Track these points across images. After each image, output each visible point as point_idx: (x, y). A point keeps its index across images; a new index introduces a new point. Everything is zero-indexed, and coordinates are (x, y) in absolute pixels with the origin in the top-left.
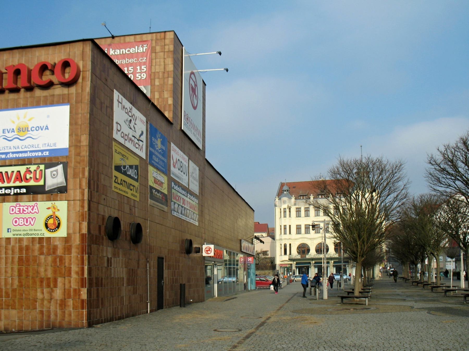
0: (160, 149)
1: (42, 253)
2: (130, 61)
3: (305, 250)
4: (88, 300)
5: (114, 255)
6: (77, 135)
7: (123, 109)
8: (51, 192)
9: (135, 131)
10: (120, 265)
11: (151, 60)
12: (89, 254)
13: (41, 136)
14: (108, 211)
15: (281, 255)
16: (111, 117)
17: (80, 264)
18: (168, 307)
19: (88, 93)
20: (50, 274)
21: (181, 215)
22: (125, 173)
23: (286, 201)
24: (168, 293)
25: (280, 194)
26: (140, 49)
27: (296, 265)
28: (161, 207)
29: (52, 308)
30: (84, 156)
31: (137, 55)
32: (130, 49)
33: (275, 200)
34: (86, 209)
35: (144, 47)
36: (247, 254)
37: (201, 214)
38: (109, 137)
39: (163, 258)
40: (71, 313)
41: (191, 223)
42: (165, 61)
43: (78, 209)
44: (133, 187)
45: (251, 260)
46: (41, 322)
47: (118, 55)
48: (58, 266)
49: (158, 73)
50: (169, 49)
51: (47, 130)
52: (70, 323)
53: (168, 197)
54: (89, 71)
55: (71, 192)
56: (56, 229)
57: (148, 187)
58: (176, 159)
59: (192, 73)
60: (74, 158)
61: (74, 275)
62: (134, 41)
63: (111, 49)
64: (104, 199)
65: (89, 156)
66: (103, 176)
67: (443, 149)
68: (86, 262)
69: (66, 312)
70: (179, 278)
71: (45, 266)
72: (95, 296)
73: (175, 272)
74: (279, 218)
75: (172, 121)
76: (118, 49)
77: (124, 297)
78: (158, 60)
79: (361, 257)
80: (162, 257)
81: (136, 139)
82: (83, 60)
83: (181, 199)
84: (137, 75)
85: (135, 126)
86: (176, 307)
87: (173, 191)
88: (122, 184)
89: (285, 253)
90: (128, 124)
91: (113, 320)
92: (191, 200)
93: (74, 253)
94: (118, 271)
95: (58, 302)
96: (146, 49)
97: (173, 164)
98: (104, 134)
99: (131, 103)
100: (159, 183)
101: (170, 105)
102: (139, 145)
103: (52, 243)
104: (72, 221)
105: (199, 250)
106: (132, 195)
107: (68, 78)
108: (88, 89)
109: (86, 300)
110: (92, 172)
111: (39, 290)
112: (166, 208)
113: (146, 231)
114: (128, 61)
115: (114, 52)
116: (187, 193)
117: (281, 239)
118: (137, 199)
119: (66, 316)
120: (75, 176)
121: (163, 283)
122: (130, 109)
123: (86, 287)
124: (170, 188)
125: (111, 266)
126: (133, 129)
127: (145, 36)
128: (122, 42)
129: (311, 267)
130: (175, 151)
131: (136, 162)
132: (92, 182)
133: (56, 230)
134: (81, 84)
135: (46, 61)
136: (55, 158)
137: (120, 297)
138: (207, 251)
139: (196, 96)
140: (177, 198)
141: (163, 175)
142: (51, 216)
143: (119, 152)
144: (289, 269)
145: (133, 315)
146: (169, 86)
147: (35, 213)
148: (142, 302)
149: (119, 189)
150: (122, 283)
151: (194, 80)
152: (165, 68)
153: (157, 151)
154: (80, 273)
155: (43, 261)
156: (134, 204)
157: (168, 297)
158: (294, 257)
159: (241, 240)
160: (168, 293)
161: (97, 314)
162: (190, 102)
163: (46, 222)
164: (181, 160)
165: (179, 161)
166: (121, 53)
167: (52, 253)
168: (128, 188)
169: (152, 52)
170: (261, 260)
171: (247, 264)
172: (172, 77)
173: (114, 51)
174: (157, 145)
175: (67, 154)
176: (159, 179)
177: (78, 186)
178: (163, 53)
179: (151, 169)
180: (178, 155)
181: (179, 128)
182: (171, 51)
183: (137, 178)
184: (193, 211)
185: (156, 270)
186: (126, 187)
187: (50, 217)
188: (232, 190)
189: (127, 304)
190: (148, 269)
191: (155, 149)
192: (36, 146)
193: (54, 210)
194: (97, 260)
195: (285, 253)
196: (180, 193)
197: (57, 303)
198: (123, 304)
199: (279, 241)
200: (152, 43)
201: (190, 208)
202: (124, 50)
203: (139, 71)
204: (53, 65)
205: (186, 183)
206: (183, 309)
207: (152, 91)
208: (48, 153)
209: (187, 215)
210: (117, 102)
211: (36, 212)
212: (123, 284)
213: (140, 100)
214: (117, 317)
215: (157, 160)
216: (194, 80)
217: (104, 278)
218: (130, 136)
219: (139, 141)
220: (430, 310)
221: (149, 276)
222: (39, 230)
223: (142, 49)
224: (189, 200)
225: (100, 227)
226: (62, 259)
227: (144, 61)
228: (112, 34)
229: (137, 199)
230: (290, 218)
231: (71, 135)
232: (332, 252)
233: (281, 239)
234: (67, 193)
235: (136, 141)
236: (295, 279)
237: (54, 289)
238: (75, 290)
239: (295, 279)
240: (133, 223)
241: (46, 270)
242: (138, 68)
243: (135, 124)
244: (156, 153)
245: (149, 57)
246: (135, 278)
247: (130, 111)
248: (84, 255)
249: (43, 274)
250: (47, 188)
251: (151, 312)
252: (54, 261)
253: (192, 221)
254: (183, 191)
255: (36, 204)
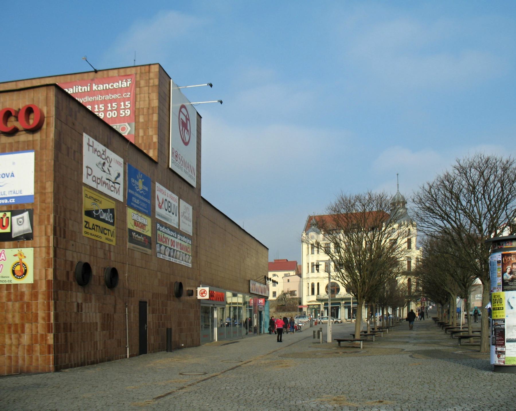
0: (141, 191)
1: (9, 300)
2: (114, 96)
3: (334, 290)
4: (54, 345)
5: (85, 300)
6: (42, 182)
7: (95, 152)
8: (17, 239)
9: (110, 174)
10: (93, 310)
11: (135, 95)
12: (56, 300)
13: (7, 184)
14: (77, 257)
15: (308, 295)
16: (80, 162)
17: (46, 310)
18: (152, 352)
19: (52, 139)
20: (17, 320)
21: (169, 257)
22: (98, 218)
23: (314, 236)
24: (152, 338)
25: (307, 229)
26: (124, 83)
27: (324, 305)
28: (143, 250)
29: (20, 354)
30: (49, 203)
31: (121, 90)
32: (114, 83)
33: (302, 235)
34: (52, 255)
35: (128, 81)
36: (258, 296)
37: (196, 255)
38: (78, 182)
39: (146, 302)
40: (38, 357)
41: (182, 265)
42: (150, 97)
43: (44, 255)
44: (107, 231)
45: (262, 302)
46: (10, 367)
47: (101, 90)
48: (25, 313)
49: (143, 109)
50: (154, 83)
51: (12, 177)
52: (37, 368)
53: (152, 239)
54: (53, 117)
55: (37, 239)
56: (22, 275)
57: (126, 231)
58: (162, 199)
59: (183, 106)
60: (40, 205)
61: (41, 321)
62: (117, 75)
63: (94, 85)
64: (73, 245)
65: (54, 203)
66: (71, 222)
67: (427, 188)
68: (52, 308)
69: (34, 357)
70: (167, 323)
71: (13, 312)
72: (63, 341)
73: (161, 316)
74: (307, 255)
75: (156, 160)
76: (101, 84)
77: (97, 341)
78: (142, 95)
79: (361, 298)
80: (145, 301)
81: (110, 182)
82: (47, 106)
83: (169, 240)
84: (121, 112)
85: (110, 168)
86: (163, 352)
87: (159, 232)
88: (94, 229)
89: (313, 293)
90: (101, 167)
91: (85, 365)
92: (182, 241)
93: (41, 299)
94: (90, 317)
95: (26, 347)
96: (130, 84)
97: (159, 205)
98: (71, 179)
99: (105, 145)
100: (140, 225)
101: (155, 143)
102: (115, 188)
103: (19, 290)
104: (39, 267)
105: (191, 293)
106: (107, 239)
107: (33, 124)
108: (52, 135)
109: (52, 345)
110: (57, 219)
111: (7, 336)
112: (149, 251)
113: (123, 276)
114: (111, 97)
115: (97, 88)
116: (177, 234)
117: (308, 278)
118: (114, 243)
119: (34, 361)
120: (41, 222)
121: (147, 327)
122: (104, 152)
123: (52, 332)
124: (154, 230)
125: (82, 311)
126: (108, 172)
127: (129, 69)
128: (105, 76)
129: (340, 308)
130: (161, 191)
131: (111, 205)
132: (58, 228)
133: (23, 277)
134: (45, 131)
135: (10, 107)
136: (21, 205)
137: (93, 342)
138: (202, 293)
139: (188, 131)
140: (164, 240)
141: (145, 217)
142: (18, 263)
143: (90, 196)
144: (317, 310)
145: (109, 360)
146: (154, 123)
147: (3, 260)
148: (120, 346)
149: (91, 234)
150: (95, 328)
151: (186, 113)
152: (149, 104)
153: (138, 192)
154: (46, 318)
155: (11, 307)
156: (110, 248)
157: (152, 342)
158: (322, 297)
159: (249, 281)
160: (152, 338)
161: (65, 359)
162: (180, 136)
163: (13, 269)
164: (168, 199)
165: (166, 202)
166: (105, 88)
167: (19, 299)
168: (101, 233)
169: (136, 87)
170: (288, 300)
171: (258, 306)
172: (156, 113)
173: (97, 86)
174: (137, 186)
175: (33, 201)
176: (141, 221)
177: (44, 233)
178: (148, 87)
179: (130, 212)
180: (165, 195)
181: (166, 166)
182: (156, 86)
183: (112, 222)
184: (184, 252)
185: (138, 314)
186: (99, 232)
187: (16, 264)
188: (238, 228)
189: (101, 348)
190: (127, 313)
191: (134, 190)
192: (3, 194)
193: (21, 257)
194: (65, 306)
195: (313, 293)
196: (166, 234)
197: (24, 349)
198: (97, 349)
199: (306, 280)
200: (136, 78)
201: (181, 249)
202: (107, 85)
203: (123, 107)
204: (18, 111)
205: (175, 224)
206: (169, 354)
207: (136, 128)
208: (15, 201)
209: (178, 257)
210: (88, 146)
211: (3, 259)
212: (97, 329)
213: (116, 141)
214: (90, 362)
215: (138, 202)
216: (186, 113)
217: (74, 323)
218: (104, 179)
219: (116, 184)
220: (413, 354)
221: (128, 321)
222: (6, 277)
223: (125, 83)
224: (180, 242)
225: (68, 273)
226: (28, 305)
227: (128, 96)
228: (95, 68)
229: (114, 243)
230: (318, 255)
231: (36, 182)
232: (343, 292)
233: (308, 278)
234: (33, 240)
235: (111, 184)
236: (322, 321)
237: (22, 335)
238: (42, 335)
239: (322, 321)
240: (108, 268)
241: (13, 317)
242: (122, 104)
243: (110, 166)
244: (137, 195)
245: (133, 92)
246: (112, 323)
247: (103, 154)
248: (51, 301)
249: (10, 321)
250: (14, 236)
251: (130, 356)
252: (22, 307)
253: (183, 263)
254: (171, 232)
255: (3, 252)
